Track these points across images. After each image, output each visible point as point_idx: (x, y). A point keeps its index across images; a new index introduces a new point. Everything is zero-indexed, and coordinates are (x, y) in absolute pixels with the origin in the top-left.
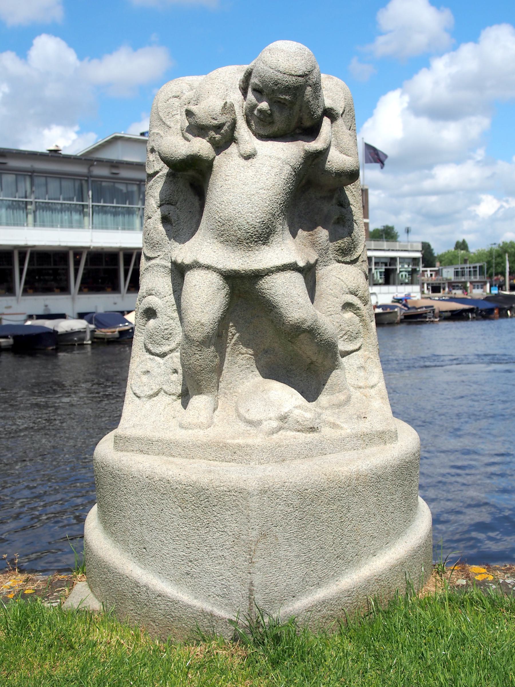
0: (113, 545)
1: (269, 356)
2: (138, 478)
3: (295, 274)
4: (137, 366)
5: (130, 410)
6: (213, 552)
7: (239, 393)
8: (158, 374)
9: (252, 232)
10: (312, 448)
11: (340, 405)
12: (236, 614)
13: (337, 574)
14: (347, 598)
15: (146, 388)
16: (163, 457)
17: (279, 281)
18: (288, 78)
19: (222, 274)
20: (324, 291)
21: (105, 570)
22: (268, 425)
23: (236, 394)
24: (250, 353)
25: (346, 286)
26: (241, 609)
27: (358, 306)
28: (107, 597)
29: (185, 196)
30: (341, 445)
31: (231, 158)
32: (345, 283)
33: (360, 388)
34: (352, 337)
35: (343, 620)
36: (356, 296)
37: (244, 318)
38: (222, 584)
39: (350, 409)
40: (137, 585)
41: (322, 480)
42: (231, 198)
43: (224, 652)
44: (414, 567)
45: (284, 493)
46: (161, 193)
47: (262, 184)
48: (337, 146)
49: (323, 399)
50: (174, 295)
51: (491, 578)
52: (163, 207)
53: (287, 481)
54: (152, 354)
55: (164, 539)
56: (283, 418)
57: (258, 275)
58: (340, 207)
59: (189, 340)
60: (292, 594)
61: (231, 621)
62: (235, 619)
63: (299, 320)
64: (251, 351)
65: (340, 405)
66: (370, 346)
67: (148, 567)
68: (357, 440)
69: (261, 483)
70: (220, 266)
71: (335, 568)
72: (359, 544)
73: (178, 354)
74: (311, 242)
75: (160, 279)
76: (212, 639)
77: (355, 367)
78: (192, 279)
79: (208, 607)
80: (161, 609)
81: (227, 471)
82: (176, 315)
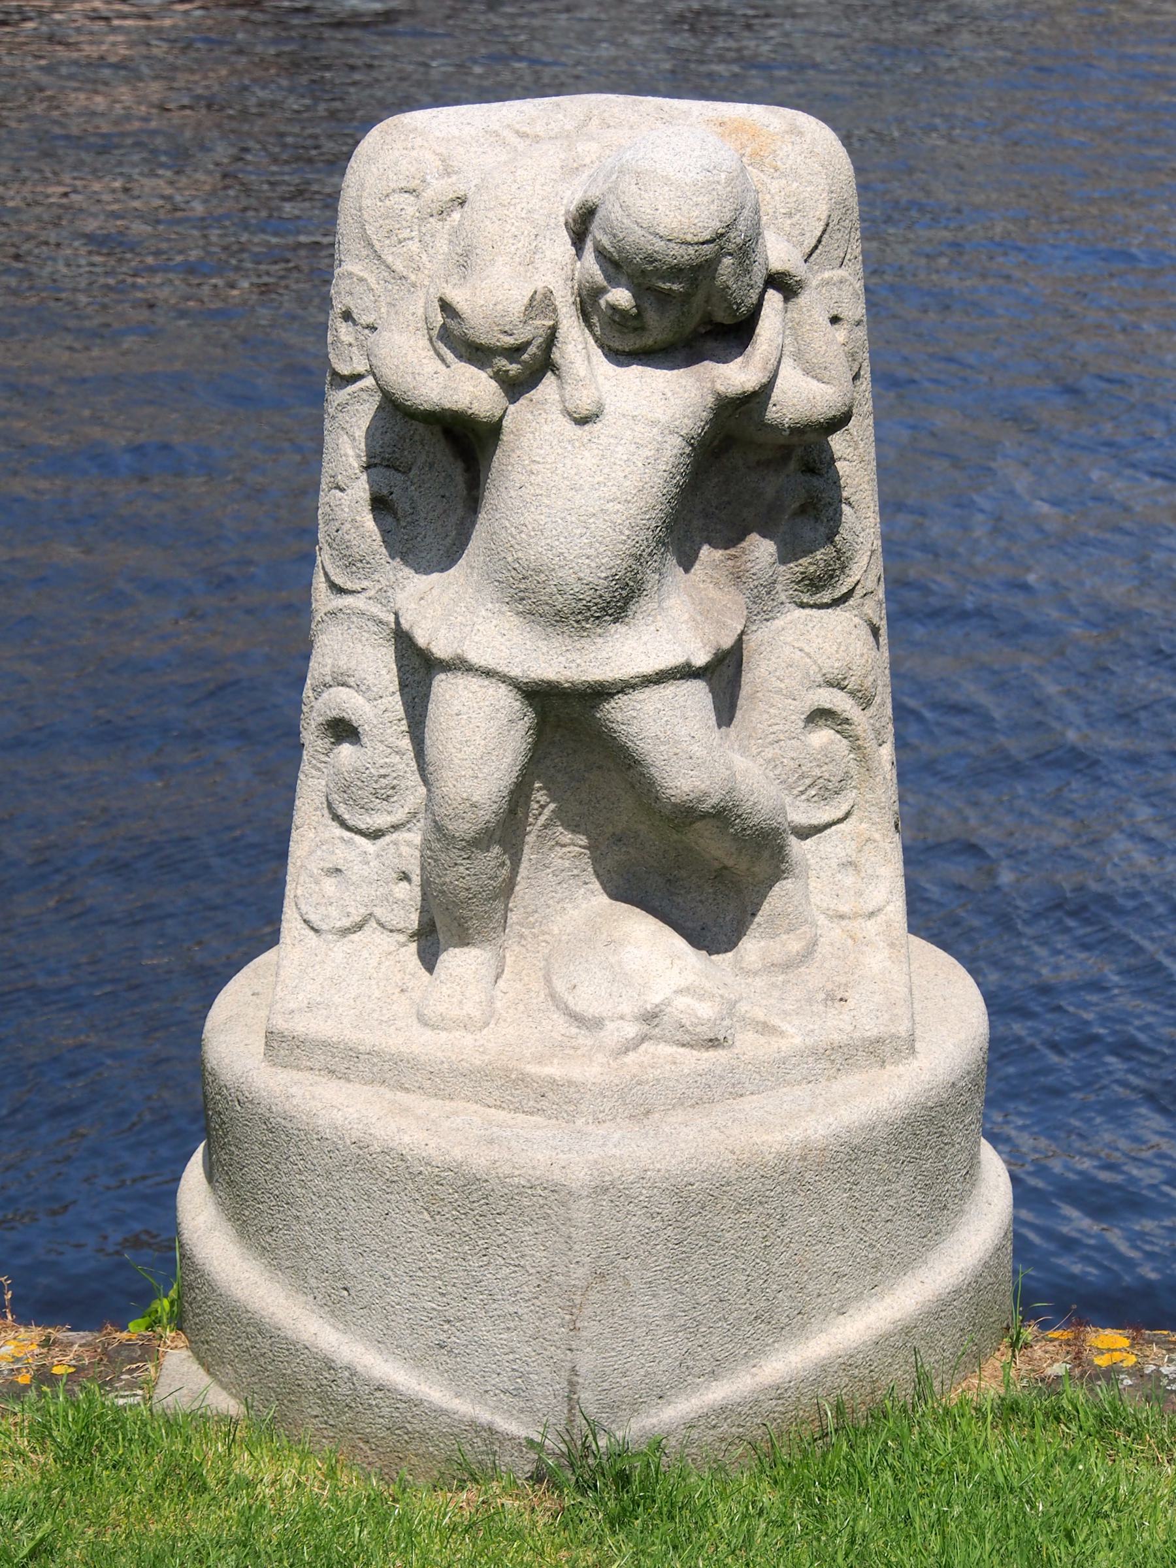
0: (267, 1274)
1: (624, 849)
2: (334, 1142)
3: (685, 686)
4: (311, 853)
5: (296, 963)
6: (495, 1306)
7: (553, 936)
8: (364, 879)
9: (588, 599)
10: (711, 1083)
11: (789, 965)
12: (541, 1430)
13: (754, 1353)
14: (774, 1402)
15: (333, 912)
16: (382, 1088)
17: (649, 708)
18: (677, 250)
19: (519, 689)
20: (762, 683)
21: (250, 1329)
22: (616, 1034)
23: (547, 937)
24: (581, 843)
25: (817, 669)
26: (553, 1420)
27: (845, 715)
28: (255, 1387)
29: (431, 456)
30: (778, 1072)
31: (544, 415)
32: (815, 662)
33: (842, 917)
34: (827, 792)
35: (764, 1447)
36: (843, 689)
37: (569, 770)
38: (513, 1370)
39: (813, 977)
40: (329, 1365)
41: (725, 1164)
42: (543, 519)
43: (517, 1504)
44: (938, 1336)
45: (644, 1191)
46: (370, 434)
47: (614, 489)
48: (798, 356)
49: (751, 947)
50: (402, 695)
51: (1131, 1360)
52: (373, 470)
53: (651, 1167)
54: (349, 829)
55: (390, 1273)
56: (651, 1017)
57: (601, 693)
58: (808, 477)
59: (444, 835)
60: (658, 1391)
61: (531, 1442)
62: (538, 1438)
63: (692, 796)
64: (583, 840)
65: (789, 965)
66: (873, 809)
67: (353, 1328)
68: (817, 1060)
69: (596, 1173)
70: (515, 672)
71: (750, 1341)
72: (805, 1291)
73: (416, 837)
74: (732, 574)
75: (368, 649)
76: (492, 1478)
77: (834, 863)
78: (451, 696)
79: (484, 1416)
80: (383, 1417)
81: (527, 1140)
82: (406, 743)
